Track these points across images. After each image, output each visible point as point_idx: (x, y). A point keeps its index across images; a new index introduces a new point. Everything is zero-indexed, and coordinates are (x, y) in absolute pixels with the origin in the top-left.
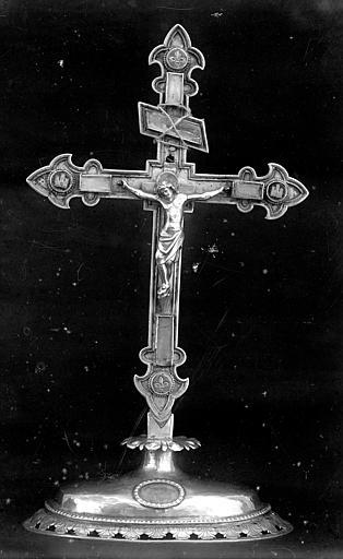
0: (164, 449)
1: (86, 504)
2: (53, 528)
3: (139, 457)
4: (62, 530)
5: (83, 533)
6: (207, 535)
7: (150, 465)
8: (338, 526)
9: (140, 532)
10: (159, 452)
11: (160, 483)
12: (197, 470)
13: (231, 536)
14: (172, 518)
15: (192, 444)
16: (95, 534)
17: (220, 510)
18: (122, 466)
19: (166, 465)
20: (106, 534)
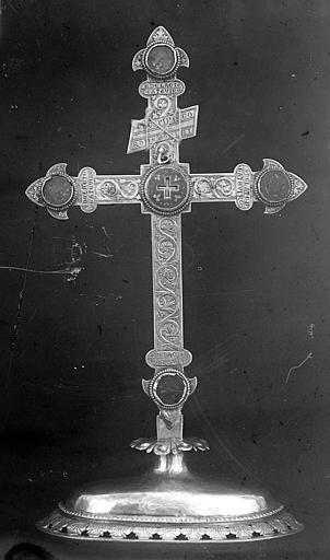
0: (175, 452)
1: (99, 504)
2: (65, 530)
3: (153, 460)
4: (75, 531)
5: (95, 533)
6: (218, 536)
7: (162, 468)
8: (107, 198)
9: (177, 532)
10: (170, 456)
11: (166, 480)
12: (208, 472)
13: (244, 535)
14: (138, 515)
15: (200, 446)
16: (107, 535)
17: (231, 511)
18: (139, 473)
19: (178, 466)
20: (119, 534)
